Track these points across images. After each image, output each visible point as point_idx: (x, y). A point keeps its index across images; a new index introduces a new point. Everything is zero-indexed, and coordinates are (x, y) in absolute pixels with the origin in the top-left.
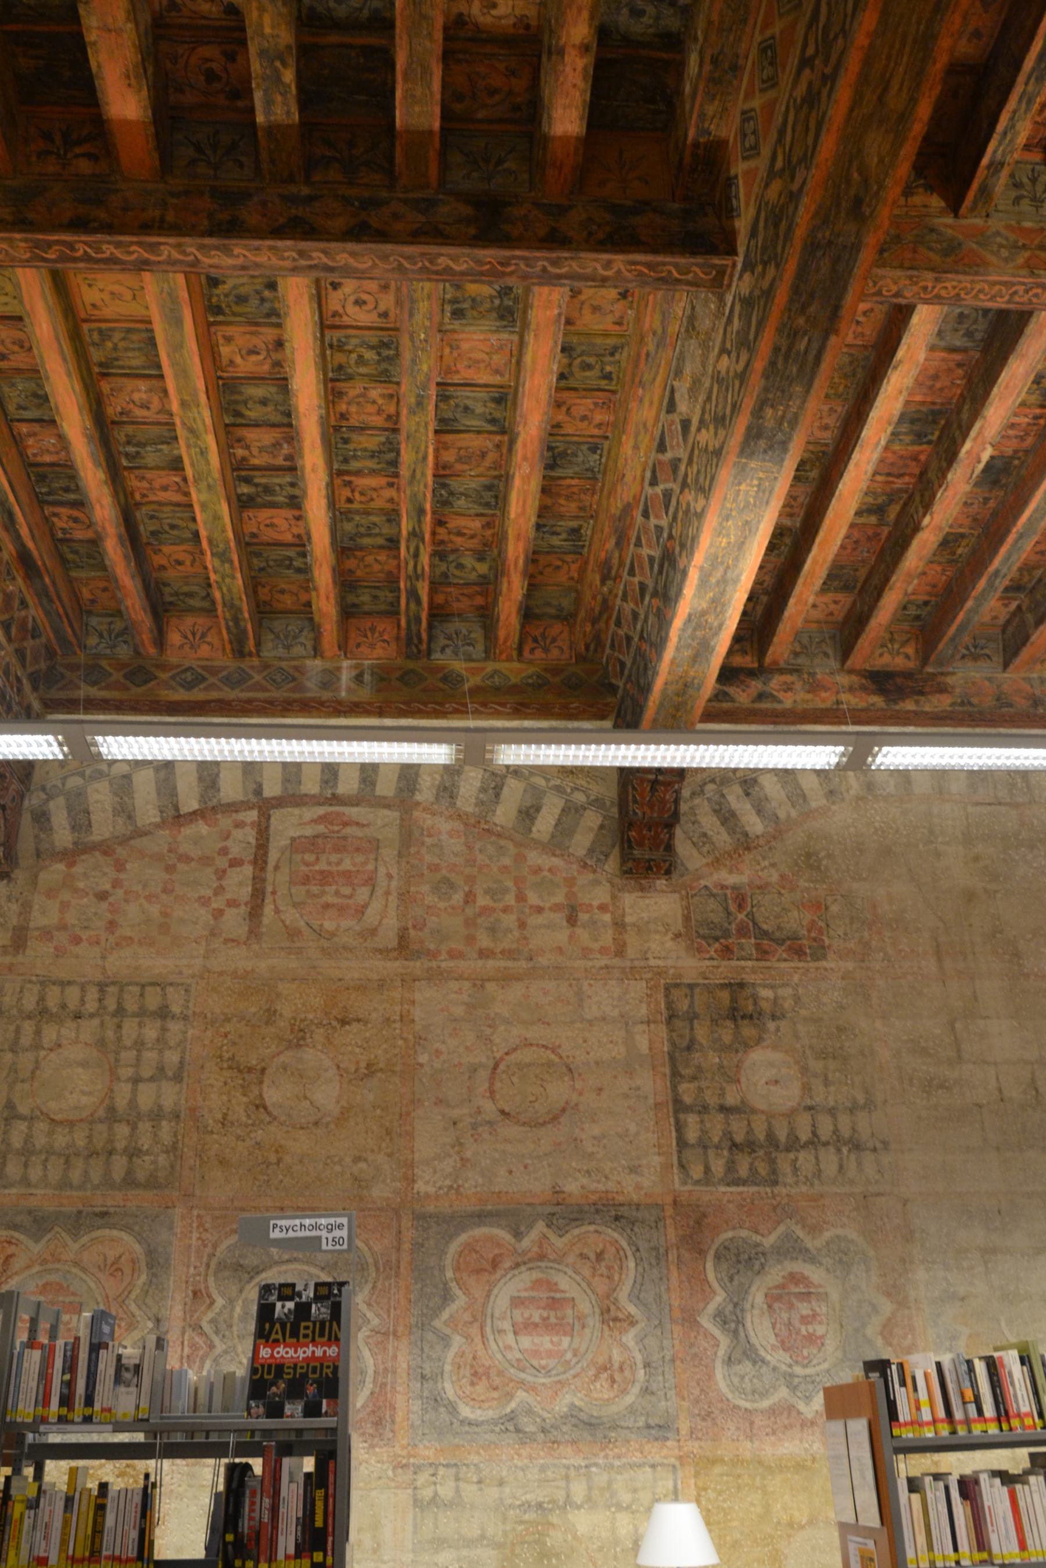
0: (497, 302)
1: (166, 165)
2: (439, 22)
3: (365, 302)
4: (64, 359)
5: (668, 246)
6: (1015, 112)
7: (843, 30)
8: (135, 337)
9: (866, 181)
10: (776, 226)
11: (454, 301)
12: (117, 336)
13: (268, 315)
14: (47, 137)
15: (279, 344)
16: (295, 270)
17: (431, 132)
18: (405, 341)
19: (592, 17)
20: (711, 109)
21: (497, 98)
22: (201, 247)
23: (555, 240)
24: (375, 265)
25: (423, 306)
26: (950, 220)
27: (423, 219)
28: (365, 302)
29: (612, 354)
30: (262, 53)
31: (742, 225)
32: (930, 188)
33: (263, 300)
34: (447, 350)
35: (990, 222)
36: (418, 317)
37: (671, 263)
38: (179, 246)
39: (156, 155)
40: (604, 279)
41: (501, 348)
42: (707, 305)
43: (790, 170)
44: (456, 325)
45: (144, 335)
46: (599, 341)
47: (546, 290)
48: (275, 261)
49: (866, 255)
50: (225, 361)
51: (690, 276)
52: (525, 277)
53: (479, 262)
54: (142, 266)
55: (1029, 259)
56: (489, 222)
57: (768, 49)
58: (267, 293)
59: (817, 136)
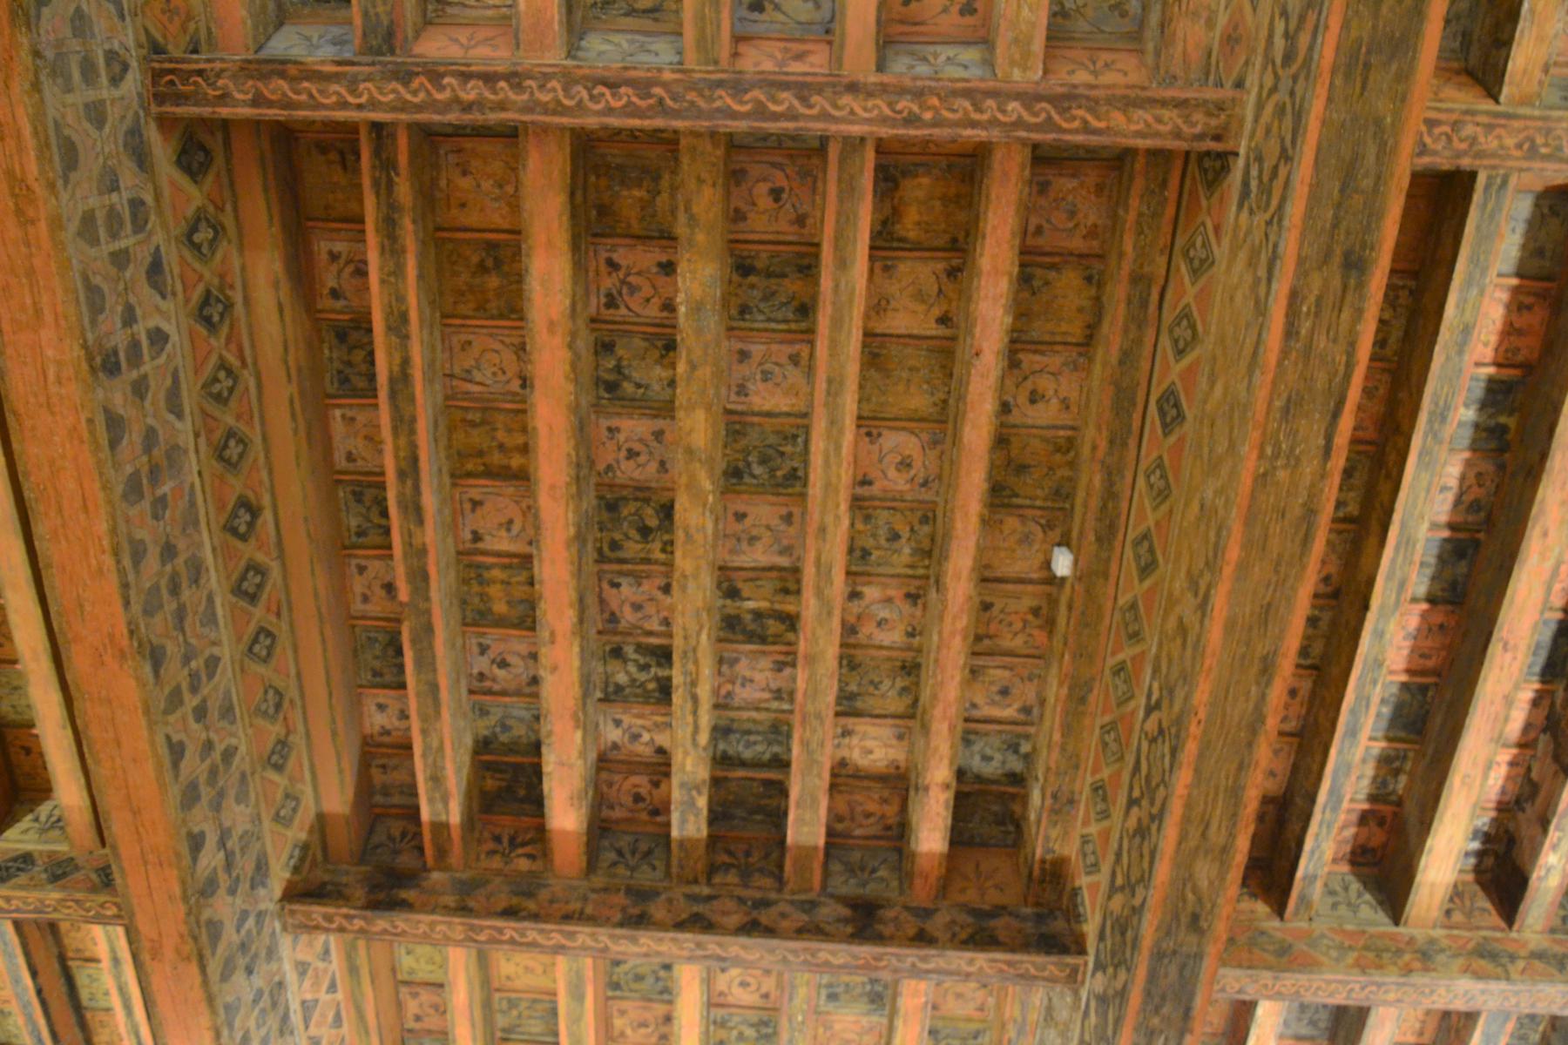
0: (868, 987)
1: (591, 867)
2: (827, 766)
3: (748, 985)
4: (473, 1026)
5: (1025, 946)
6: (1317, 835)
7: (1163, 780)
8: (539, 1006)
9: (1200, 900)
10: (1123, 934)
11: (830, 985)
12: (524, 1005)
13: (661, 993)
14: (498, 839)
15: (668, 1019)
16: (690, 959)
17: (816, 848)
18: (784, 1023)
19: (951, 764)
20: (1054, 833)
21: (872, 820)
22: (611, 937)
23: (923, 939)
24: (762, 957)
25: (802, 992)
26: (1276, 923)
27: (805, 918)
28: (748, 985)
29: (975, 1038)
30: (682, 785)
31: (1090, 928)
32: (1253, 895)
33: (658, 979)
34: (821, 1030)
35: (1314, 925)
36: (797, 1001)
37: (1030, 962)
38: (592, 935)
39: (584, 858)
40: (968, 975)
41: (871, 1029)
42: (1063, 1001)
43: (1130, 887)
44: (831, 1007)
45: (548, 1005)
46: (962, 1025)
47: (913, 982)
48: (675, 950)
49: (1207, 963)
50: (616, 1033)
51: (1046, 974)
52: (896, 971)
53: (855, 957)
54: (559, 949)
55: (1357, 960)
56: (864, 922)
57: (1097, 788)
58: (662, 973)
59: (1151, 863)
